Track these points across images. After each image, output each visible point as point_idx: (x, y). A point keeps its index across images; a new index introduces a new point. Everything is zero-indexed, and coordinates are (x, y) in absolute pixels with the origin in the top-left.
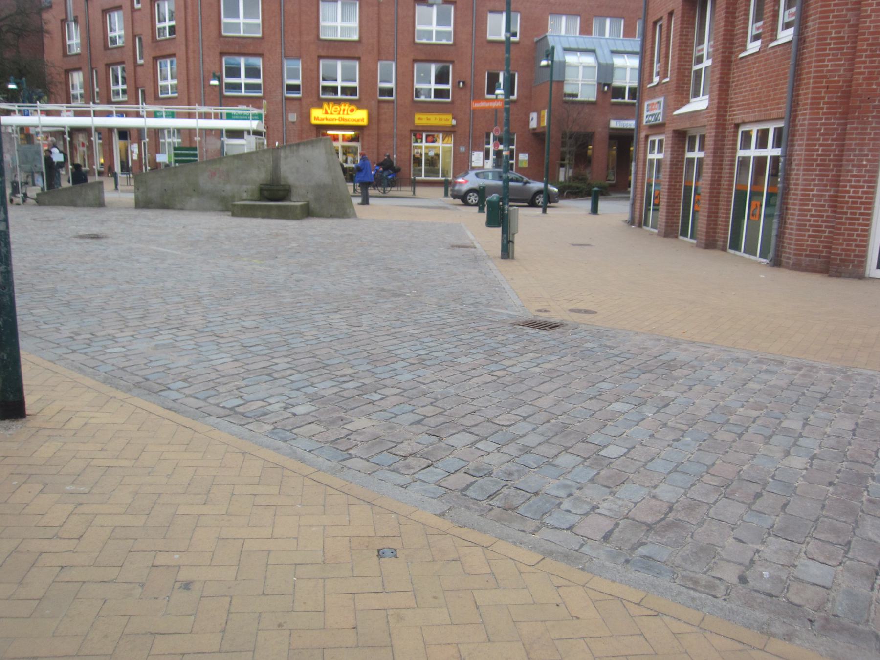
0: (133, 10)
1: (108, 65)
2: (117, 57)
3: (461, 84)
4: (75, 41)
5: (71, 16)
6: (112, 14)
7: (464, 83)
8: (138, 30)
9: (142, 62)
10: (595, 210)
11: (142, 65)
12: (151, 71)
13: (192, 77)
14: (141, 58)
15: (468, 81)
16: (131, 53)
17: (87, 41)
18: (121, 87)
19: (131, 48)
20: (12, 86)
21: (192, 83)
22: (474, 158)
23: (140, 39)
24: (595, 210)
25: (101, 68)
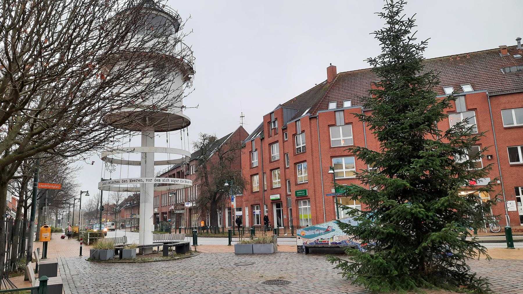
0: (285, 168)
1: (271, 170)
2: (275, 165)
3: (490, 157)
4: (256, 162)
5: (254, 149)
6: (273, 145)
7: (491, 156)
8: (286, 151)
9: (290, 193)
10: (331, 64)
11: (288, 168)
12: (293, 170)
13: (315, 171)
14: (286, 138)
15: (494, 155)
16: (283, 163)
17: (262, 160)
18: (277, 180)
19: (283, 160)
20: (227, 184)
21: (315, 174)
22: (508, 205)
23: (287, 155)
24: (331, 64)
25: (268, 172)
